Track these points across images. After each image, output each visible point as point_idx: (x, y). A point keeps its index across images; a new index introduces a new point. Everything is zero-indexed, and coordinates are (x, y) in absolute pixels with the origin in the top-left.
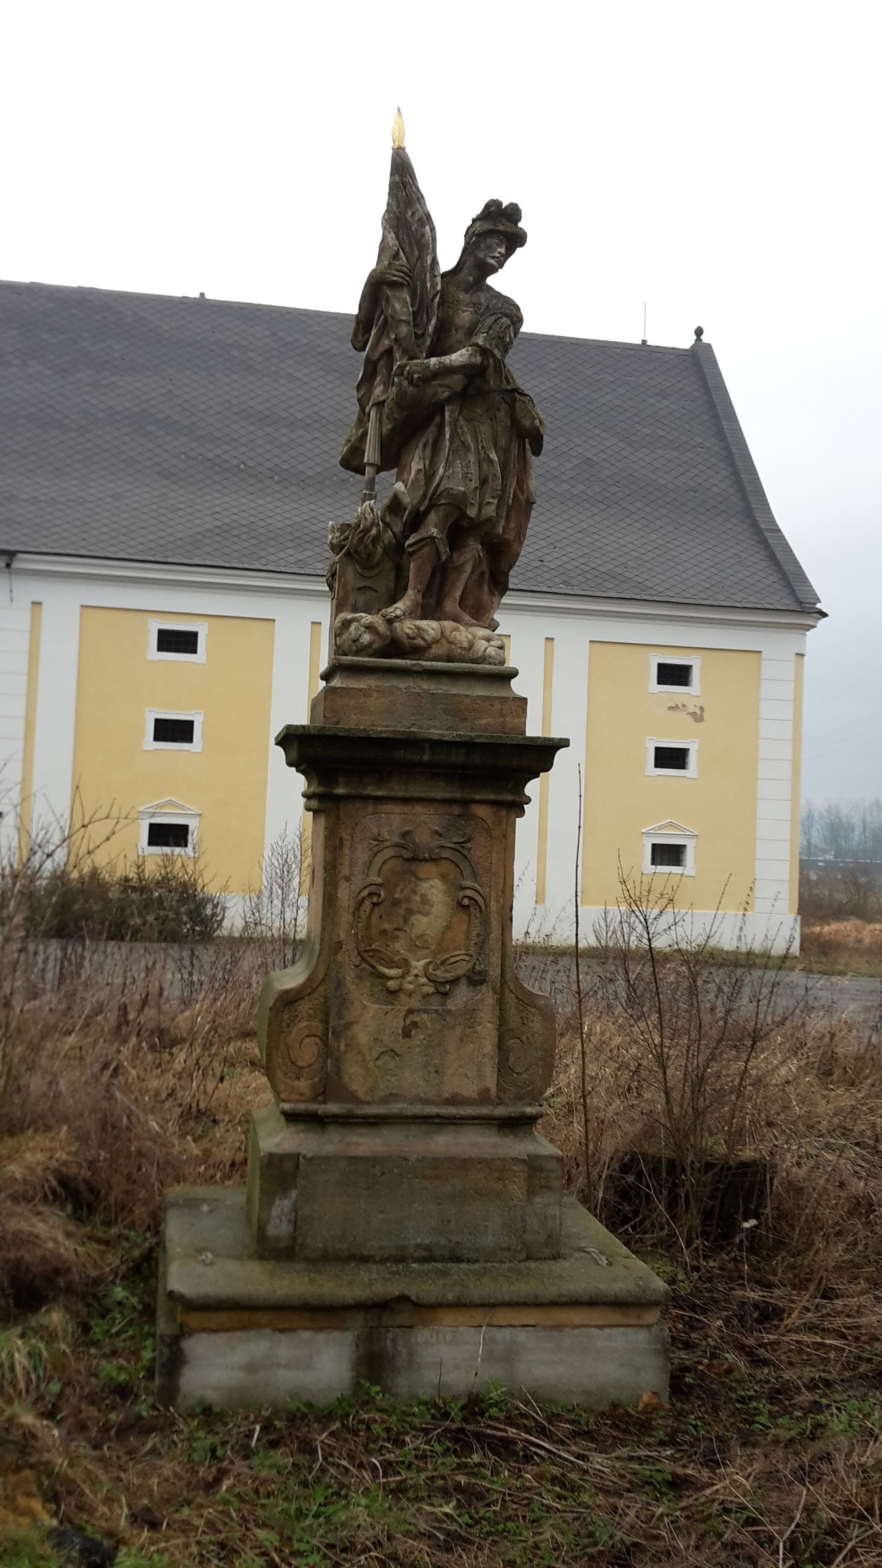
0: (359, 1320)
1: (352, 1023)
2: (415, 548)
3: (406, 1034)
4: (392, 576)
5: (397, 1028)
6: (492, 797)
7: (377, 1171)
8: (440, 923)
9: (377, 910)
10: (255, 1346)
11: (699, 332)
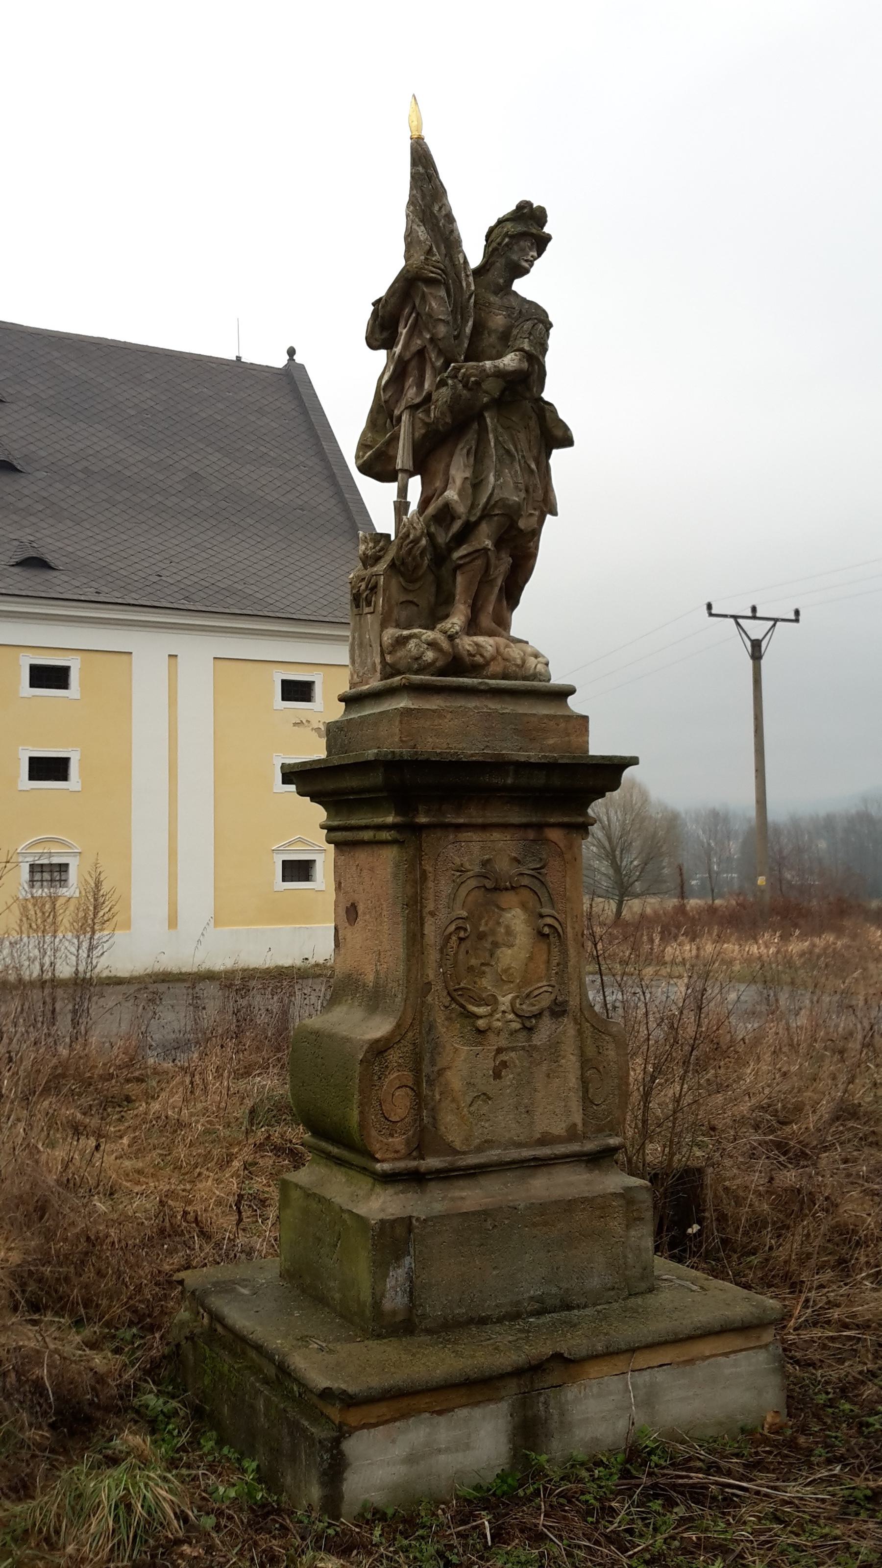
0: (512, 1387)
1: (444, 1069)
2: (467, 560)
3: (497, 1075)
4: (433, 589)
5: (488, 1069)
6: (566, 819)
7: (489, 1225)
8: (524, 955)
9: (463, 946)
10: (414, 1434)
11: (291, 352)
